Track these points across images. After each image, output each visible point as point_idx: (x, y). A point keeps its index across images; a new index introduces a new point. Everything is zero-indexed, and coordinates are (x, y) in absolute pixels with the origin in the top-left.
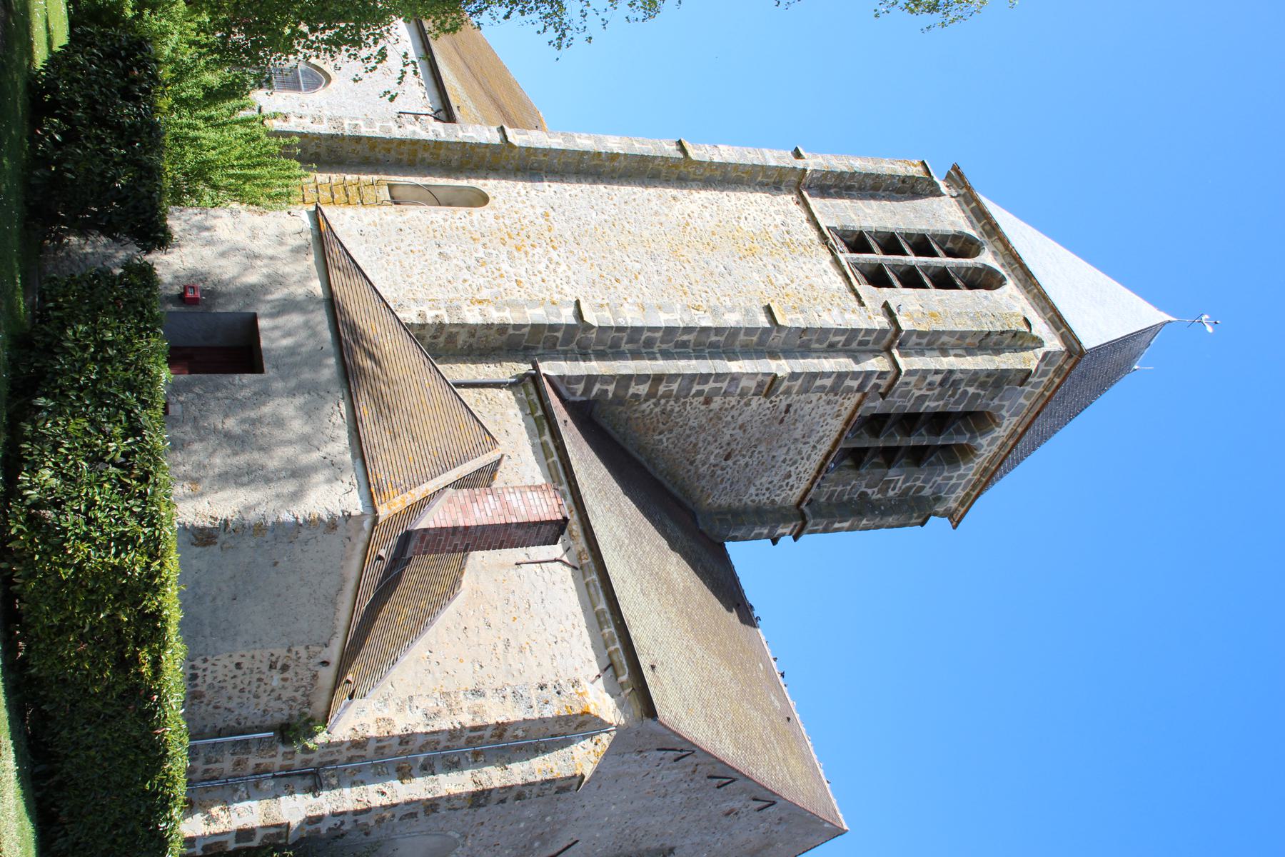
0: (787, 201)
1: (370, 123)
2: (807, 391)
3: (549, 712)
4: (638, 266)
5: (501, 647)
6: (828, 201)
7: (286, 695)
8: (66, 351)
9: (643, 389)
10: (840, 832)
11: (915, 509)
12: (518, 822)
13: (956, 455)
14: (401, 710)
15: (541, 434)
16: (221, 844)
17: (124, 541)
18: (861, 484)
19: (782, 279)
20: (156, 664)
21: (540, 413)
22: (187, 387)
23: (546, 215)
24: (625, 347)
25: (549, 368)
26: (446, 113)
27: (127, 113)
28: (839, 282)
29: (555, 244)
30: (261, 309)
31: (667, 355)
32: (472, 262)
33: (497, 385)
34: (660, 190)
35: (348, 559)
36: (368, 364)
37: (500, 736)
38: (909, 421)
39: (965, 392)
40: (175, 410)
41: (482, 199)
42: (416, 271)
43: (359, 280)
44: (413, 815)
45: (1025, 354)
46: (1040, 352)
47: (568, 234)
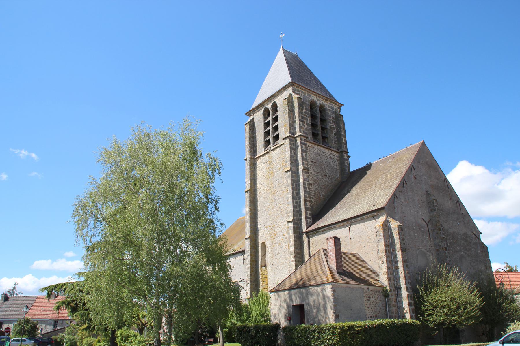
0: (258, 162)
1: (247, 272)
2: (307, 159)
3: (382, 234)
5: (369, 244)
6: (257, 150)
7: (376, 296)
8: (300, 343)
9: (308, 204)
10: (423, 143)
11: (339, 119)
12: (415, 236)
13: (322, 109)
14: (382, 269)
15: (320, 232)
16: (412, 310)
17: (333, 333)
18: (332, 136)
19: (279, 165)
20: (359, 327)
22: (308, 320)
23: (267, 227)
24: (298, 209)
25: (304, 230)
26: (243, 252)
27: (253, 332)
28: (278, 149)
30: (292, 304)
31: (300, 198)
32: (279, 247)
33: (309, 242)
34: (258, 197)
35: (342, 286)
36: (302, 281)
37: (388, 245)
38: (314, 126)
39: (305, 112)
40: (312, 322)
41: (264, 244)
43: (284, 283)
44: (407, 266)
45: (294, 99)
46: (293, 94)
47: (271, 222)
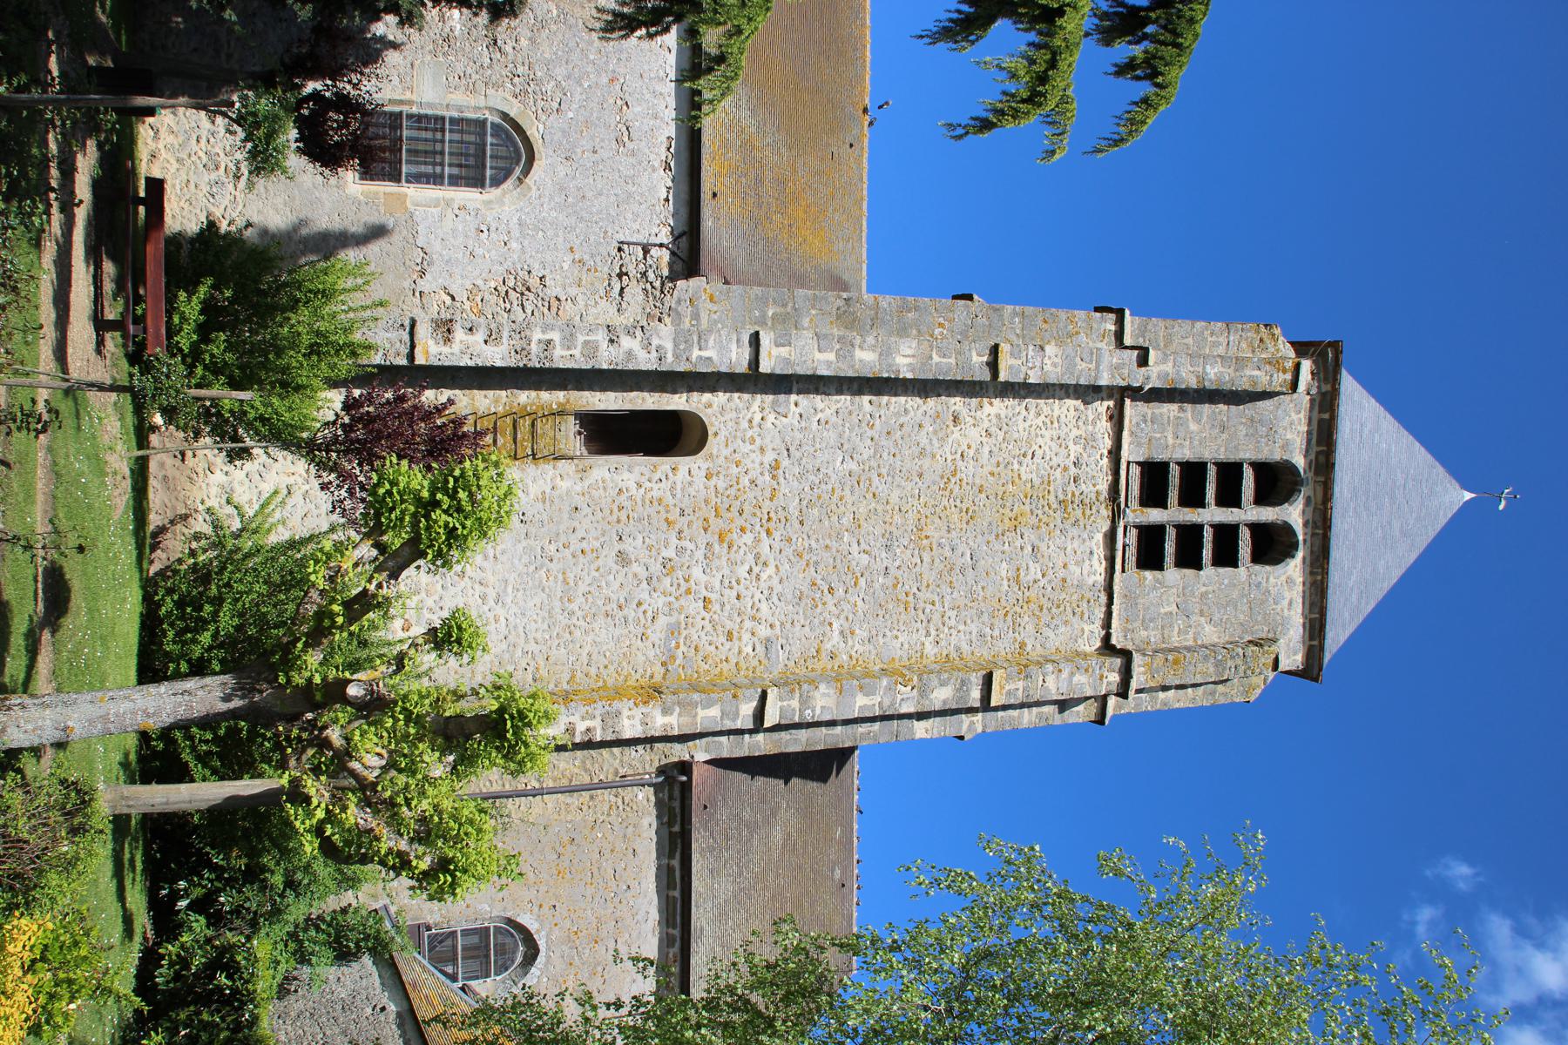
4: (865, 559)
21: (677, 828)
29: (771, 525)
42: (583, 588)
